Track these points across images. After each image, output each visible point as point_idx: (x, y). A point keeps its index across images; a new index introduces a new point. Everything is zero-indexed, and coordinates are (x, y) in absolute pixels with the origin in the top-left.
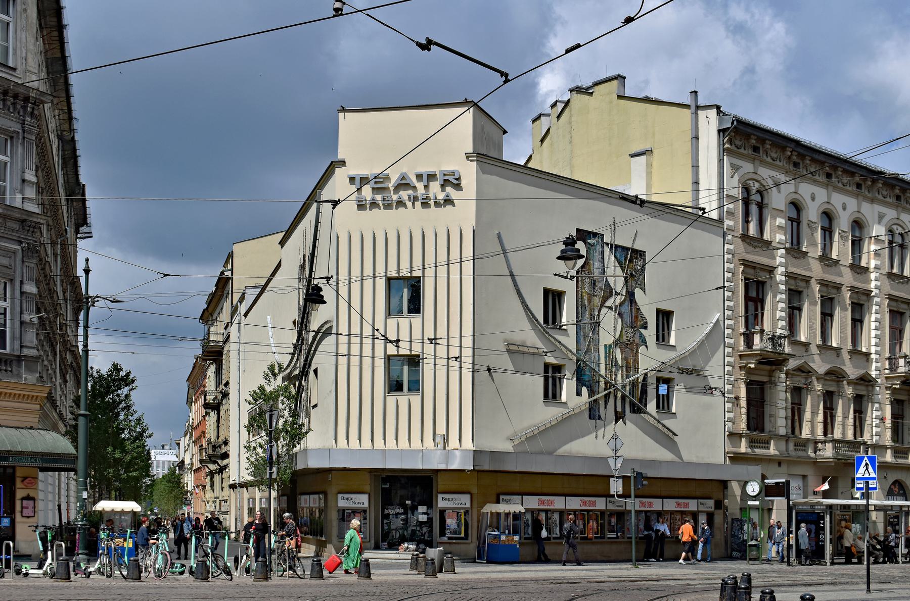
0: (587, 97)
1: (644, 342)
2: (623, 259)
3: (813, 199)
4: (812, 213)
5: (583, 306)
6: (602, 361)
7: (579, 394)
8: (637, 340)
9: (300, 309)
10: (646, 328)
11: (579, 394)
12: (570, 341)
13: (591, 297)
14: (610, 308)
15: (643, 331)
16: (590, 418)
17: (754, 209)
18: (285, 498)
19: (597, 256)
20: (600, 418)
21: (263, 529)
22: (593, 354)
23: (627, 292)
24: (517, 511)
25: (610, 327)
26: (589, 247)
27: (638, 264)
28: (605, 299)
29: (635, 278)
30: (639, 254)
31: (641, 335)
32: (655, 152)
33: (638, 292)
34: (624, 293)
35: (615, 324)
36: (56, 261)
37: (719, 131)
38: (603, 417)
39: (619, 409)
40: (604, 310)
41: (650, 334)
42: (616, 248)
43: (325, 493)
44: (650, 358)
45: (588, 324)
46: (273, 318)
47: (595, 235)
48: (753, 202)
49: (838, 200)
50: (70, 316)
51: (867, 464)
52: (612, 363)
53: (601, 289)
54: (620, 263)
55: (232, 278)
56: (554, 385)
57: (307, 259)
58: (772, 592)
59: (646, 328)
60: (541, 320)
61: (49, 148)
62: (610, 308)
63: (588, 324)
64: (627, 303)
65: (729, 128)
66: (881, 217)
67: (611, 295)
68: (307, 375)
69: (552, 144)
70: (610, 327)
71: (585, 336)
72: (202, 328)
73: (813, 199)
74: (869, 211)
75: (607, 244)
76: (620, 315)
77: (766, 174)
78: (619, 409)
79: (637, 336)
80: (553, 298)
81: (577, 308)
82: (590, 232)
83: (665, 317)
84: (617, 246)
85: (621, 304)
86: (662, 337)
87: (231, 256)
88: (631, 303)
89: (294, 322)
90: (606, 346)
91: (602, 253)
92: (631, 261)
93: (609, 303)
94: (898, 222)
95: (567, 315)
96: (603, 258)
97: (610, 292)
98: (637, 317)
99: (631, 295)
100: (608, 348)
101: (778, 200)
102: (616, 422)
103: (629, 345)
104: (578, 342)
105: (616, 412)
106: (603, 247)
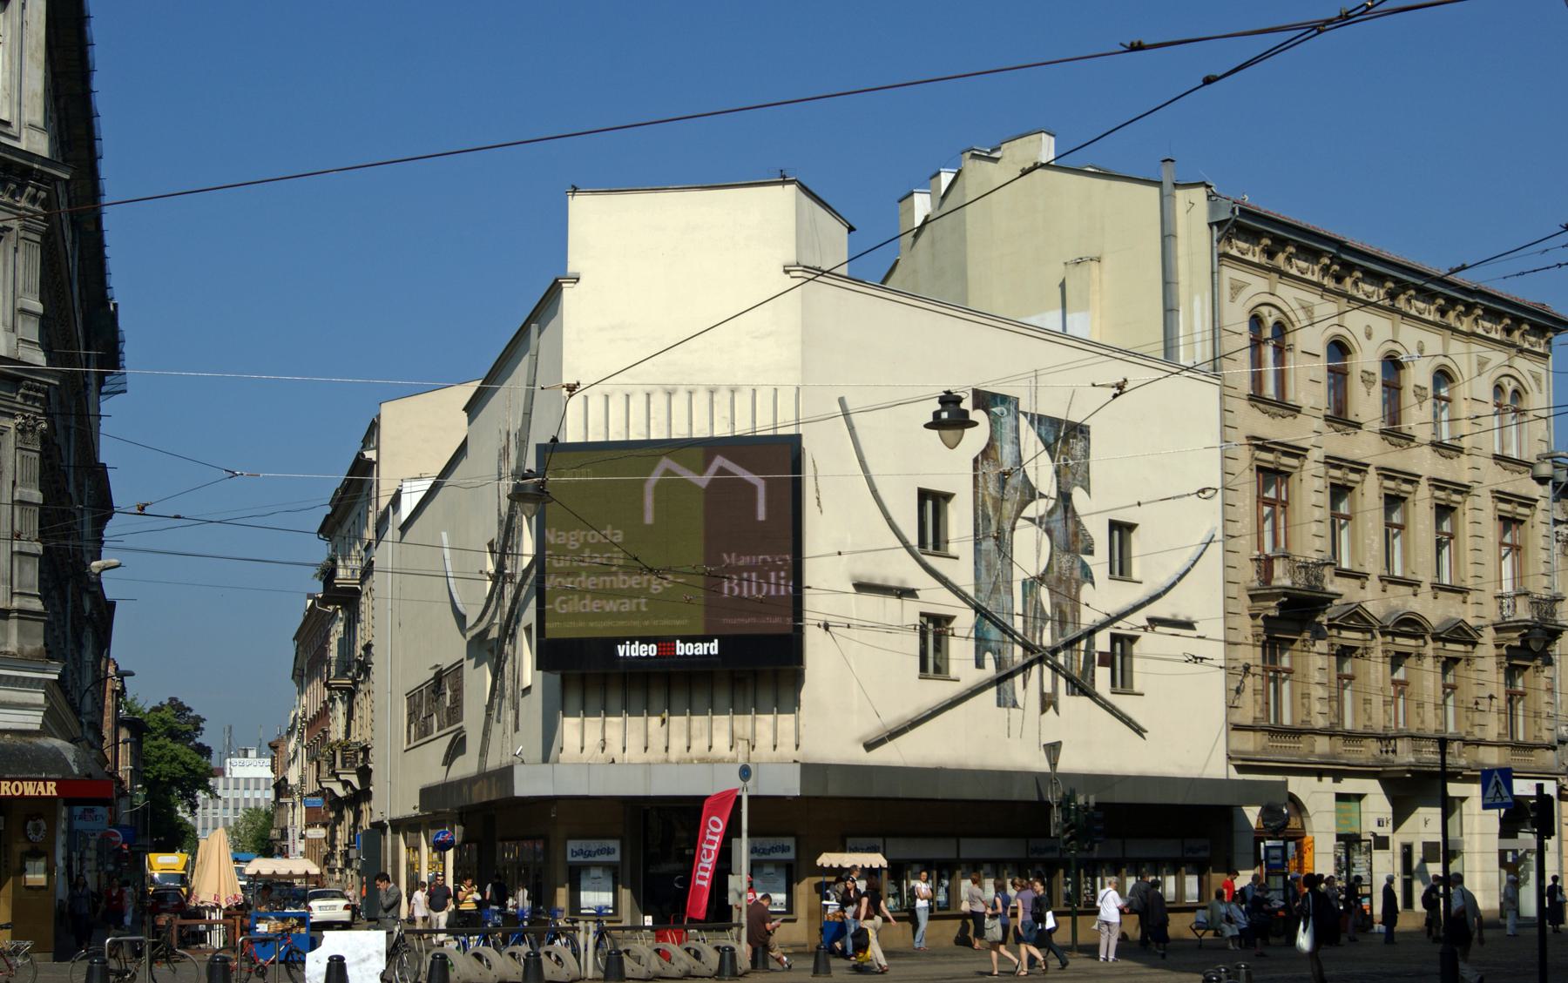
0: (990, 165)
1: (1088, 576)
2: (1051, 439)
3: (1369, 336)
4: (1366, 359)
5: (987, 518)
6: (1018, 608)
7: (979, 664)
8: (1077, 573)
9: (500, 522)
10: (1091, 553)
11: (979, 664)
12: (962, 572)
13: (999, 502)
14: (1032, 520)
15: (1087, 559)
16: (999, 705)
17: (1268, 352)
18: (474, 846)
19: (1008, 433)
20: (1015, 705)
21: (1527, 594)
22: (1005, 598)
23: (1059, 492)
24: (876, 866)
25: (1030, 550)
26: (994, 422)
27: (1077, 446)
28: (1023, 505)
29: (1072, 475)
30: (1079, 431)
31: (1084, 566)
32: (1106, 261)
33: (1078, 495)
34: (1054, 494)
35: (1039, 544)
36: (68, 439)
37: (1211, 225)
38: (1020, 703)
39: (1048, 689)
40: (1020, 522)
41: (1098, 562)
42: (1038, 420)
43: (545, 839)
44: (1101, 598)
45: (993, 537)
46: (451, 537)
47: (1004, 399)
48: (1270, 336)
49: (1410, 338)
50: (88, 530)
51: (1497, 783)
52: (1035, 615)
53: (1016, 489)
54: (1048, 447)
55: (377, 462)
56: (937, 650)
57: (512, 437)
58: (553, 449)
59: (1091, 553)
60: (914, 540)
61: (59, 238)
62: (1032, 520)
63: (993, 537)
64: (1059, 513)
65: (1226, 221)
66: (1482, 364)
67: (1033, 498)
68: (513, 635)
69: (933, 243)
70: (1030, 550)
71: (989, 567)
72: (321, 551)
73: (1369, 336)
74: (1462, 356)
75: (1025, 414)
76: (1049, 532)
77: (1290, 296)
78: (1048, 689)
79: (1077, 565)
80: (933, 502)
81: (976, 520)
82: (994, 395)
83: (1121, 530)
84: (1041, 418)
85: (1051, 513)
86: (1121, 568)
87: (374, 426)
88: (1066, 511)
89: (491, 545)
90: (1024, 583)
91: (1017, 429)
92: (1066, 442)
93: (1030, 511)
94: (1511, 372)
95: (960, 521)
96: (1018, 438)
97: (1031, 494)
98: (1076, 534)
99: (1065, 498)
100: (1030, 586)
101: (1310, 340)
102: (1043, 711)
103: (1064, 581)
104: (977, 577)
105: (1043, 694)
106: (1017, 419)
